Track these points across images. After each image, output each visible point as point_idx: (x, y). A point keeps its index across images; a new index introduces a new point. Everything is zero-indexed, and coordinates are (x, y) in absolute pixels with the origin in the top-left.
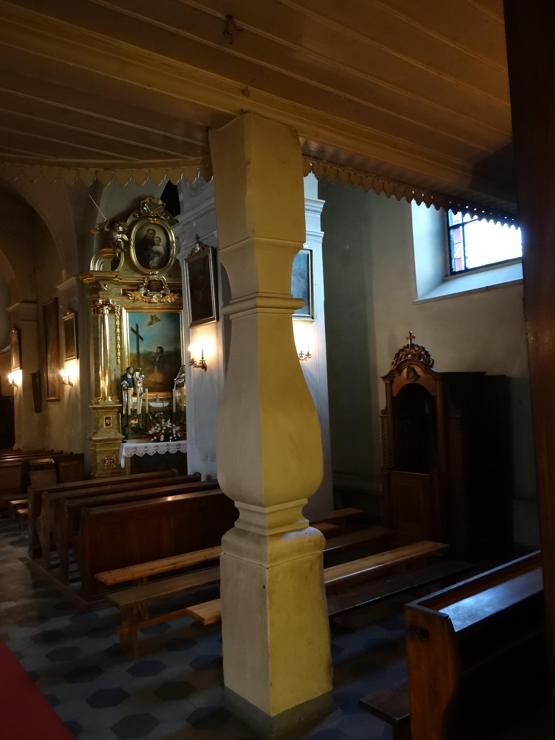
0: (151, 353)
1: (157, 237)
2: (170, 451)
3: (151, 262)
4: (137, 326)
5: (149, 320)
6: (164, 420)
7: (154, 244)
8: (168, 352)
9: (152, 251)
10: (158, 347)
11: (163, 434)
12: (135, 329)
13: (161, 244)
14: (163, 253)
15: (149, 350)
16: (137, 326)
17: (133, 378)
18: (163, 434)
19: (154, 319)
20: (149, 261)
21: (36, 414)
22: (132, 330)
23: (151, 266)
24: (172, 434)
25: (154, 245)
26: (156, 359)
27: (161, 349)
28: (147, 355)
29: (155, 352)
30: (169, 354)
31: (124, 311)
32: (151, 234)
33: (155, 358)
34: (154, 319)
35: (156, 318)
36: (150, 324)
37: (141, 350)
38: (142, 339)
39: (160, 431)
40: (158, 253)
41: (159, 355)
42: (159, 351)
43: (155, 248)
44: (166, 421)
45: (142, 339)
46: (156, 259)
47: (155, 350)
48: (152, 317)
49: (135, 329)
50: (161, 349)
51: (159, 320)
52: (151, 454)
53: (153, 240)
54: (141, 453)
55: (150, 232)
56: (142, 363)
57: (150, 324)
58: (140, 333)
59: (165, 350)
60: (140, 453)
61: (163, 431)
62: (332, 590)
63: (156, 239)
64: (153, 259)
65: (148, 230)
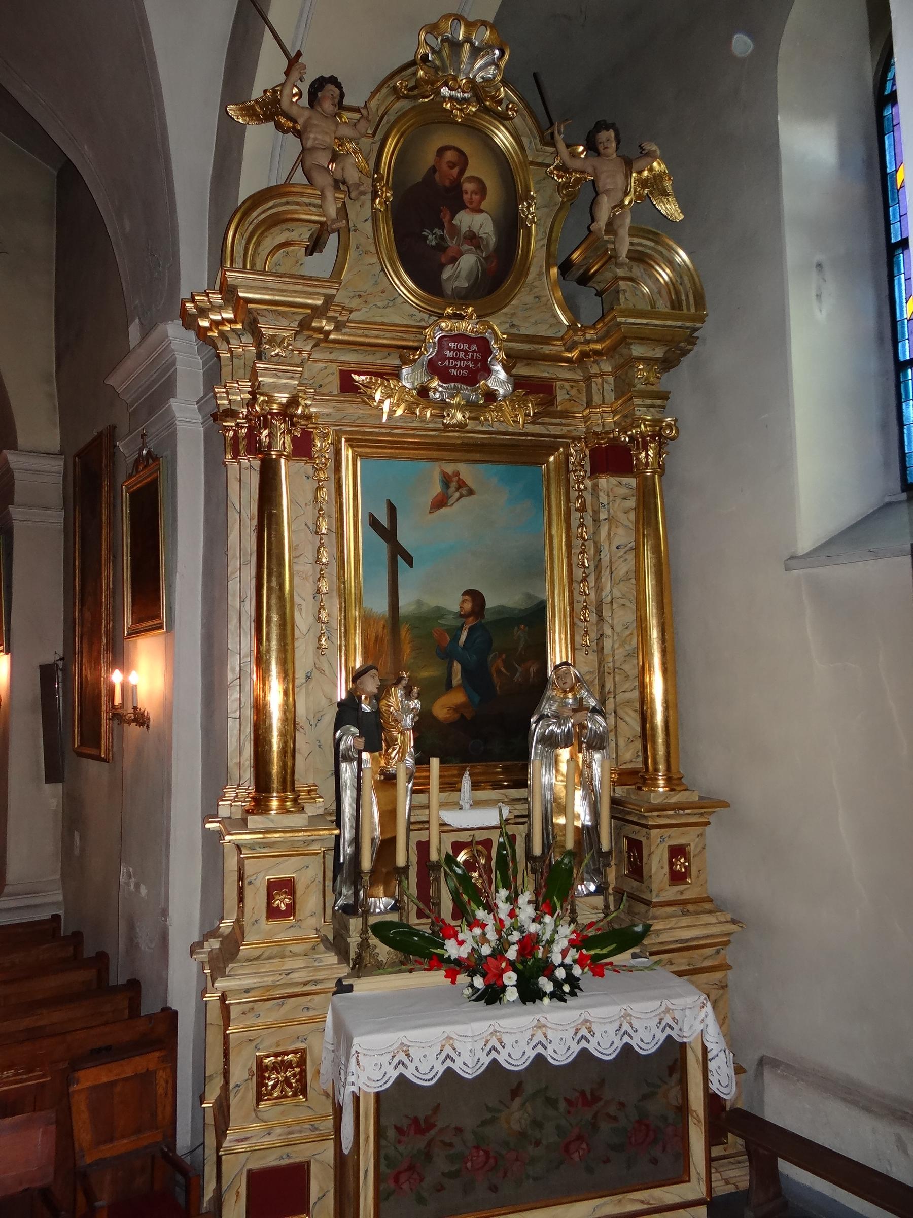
0: (439, 613)
1: (472, 179)
2: (548, 1054)
3: (447, 273)
4: (392, 510)
5: (437, 488)
6: (503, 893)
7: (458, 205)
8: (500, 610)
9: (455, 231)
10: (467, 593)
11: (512, 965)
12: (384, 521)
13: (483, 206)
14: (493, 240)
15: (432, 602)
16: (392, 510)
17: (377, 713)
18: (512, 965)
19: (454, 485)
20: (442, 266)
21: (48, 787)
22: (374, 523)
23: (449, 288)
24: (548, 969)
25: (463, 206)
26: (456, 638)
27: (475, 596)
28: (427, 620)
29: (456, 608)
30: (508, 620)
31: (347, 453)
32: (452, 165)
33: (455, 633)
34: (454, 485)
35: (461, 484)
36: (440, 503)
37: (406, 602)
38: (409, 560)
39: (499, 953)
40: (473, 239)
41: (471, 621)
42: (468, 606)
43: (465, 220)
44: (512, 900)
45: (409, 560)
46: (468, 261)
47: (453, 602)
48: (446, 480)
49: (384, 521)
50: (475, 596)
51: (471, 492)
52: (469, 1073)
53: (456, 187)
54: (425, 1070)
55: (450, 156)
56: (407, 650)
57: (440, 503)
58: (404, 537)
59: (491, 603)
60: (424, 1068)
61: (512, 953)
62: (429, 771)
63: (468, 187)
64: (454, 260)
65: (441, 151)
